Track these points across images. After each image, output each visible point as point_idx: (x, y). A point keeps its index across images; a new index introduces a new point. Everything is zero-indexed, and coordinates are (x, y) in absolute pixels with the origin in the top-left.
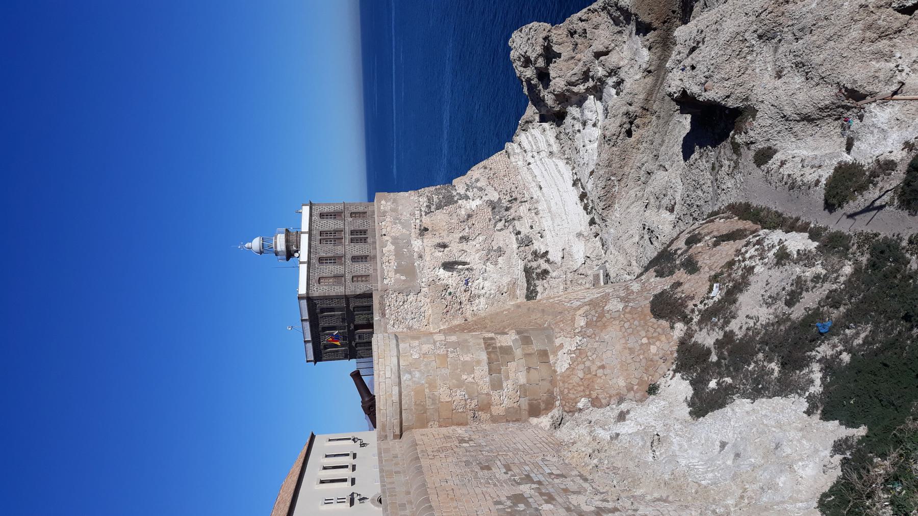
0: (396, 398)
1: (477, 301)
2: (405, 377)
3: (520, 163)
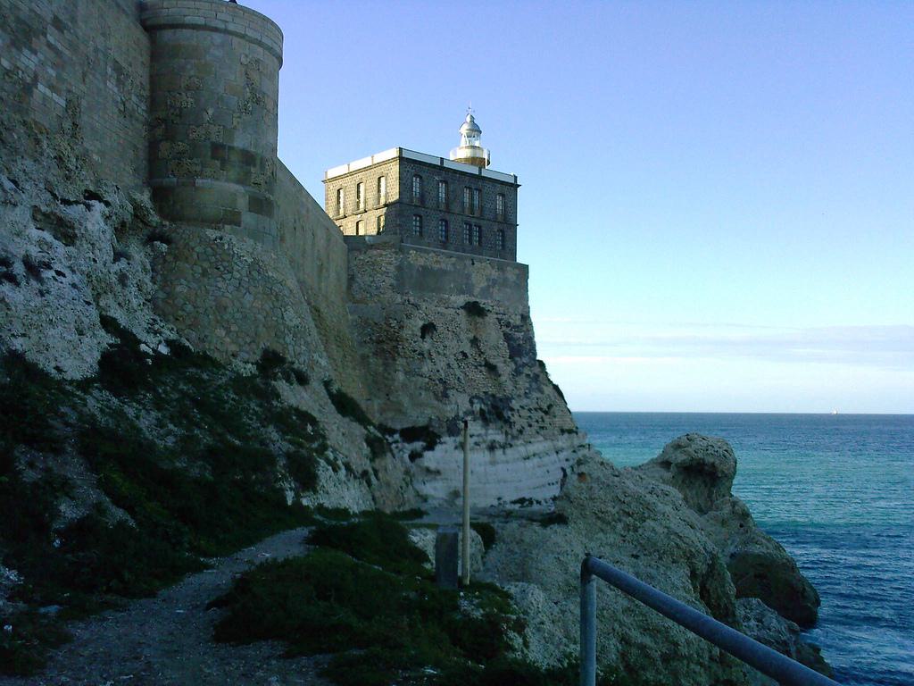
0: (188, 20)
2: (218, 38)
3: (560, 444)
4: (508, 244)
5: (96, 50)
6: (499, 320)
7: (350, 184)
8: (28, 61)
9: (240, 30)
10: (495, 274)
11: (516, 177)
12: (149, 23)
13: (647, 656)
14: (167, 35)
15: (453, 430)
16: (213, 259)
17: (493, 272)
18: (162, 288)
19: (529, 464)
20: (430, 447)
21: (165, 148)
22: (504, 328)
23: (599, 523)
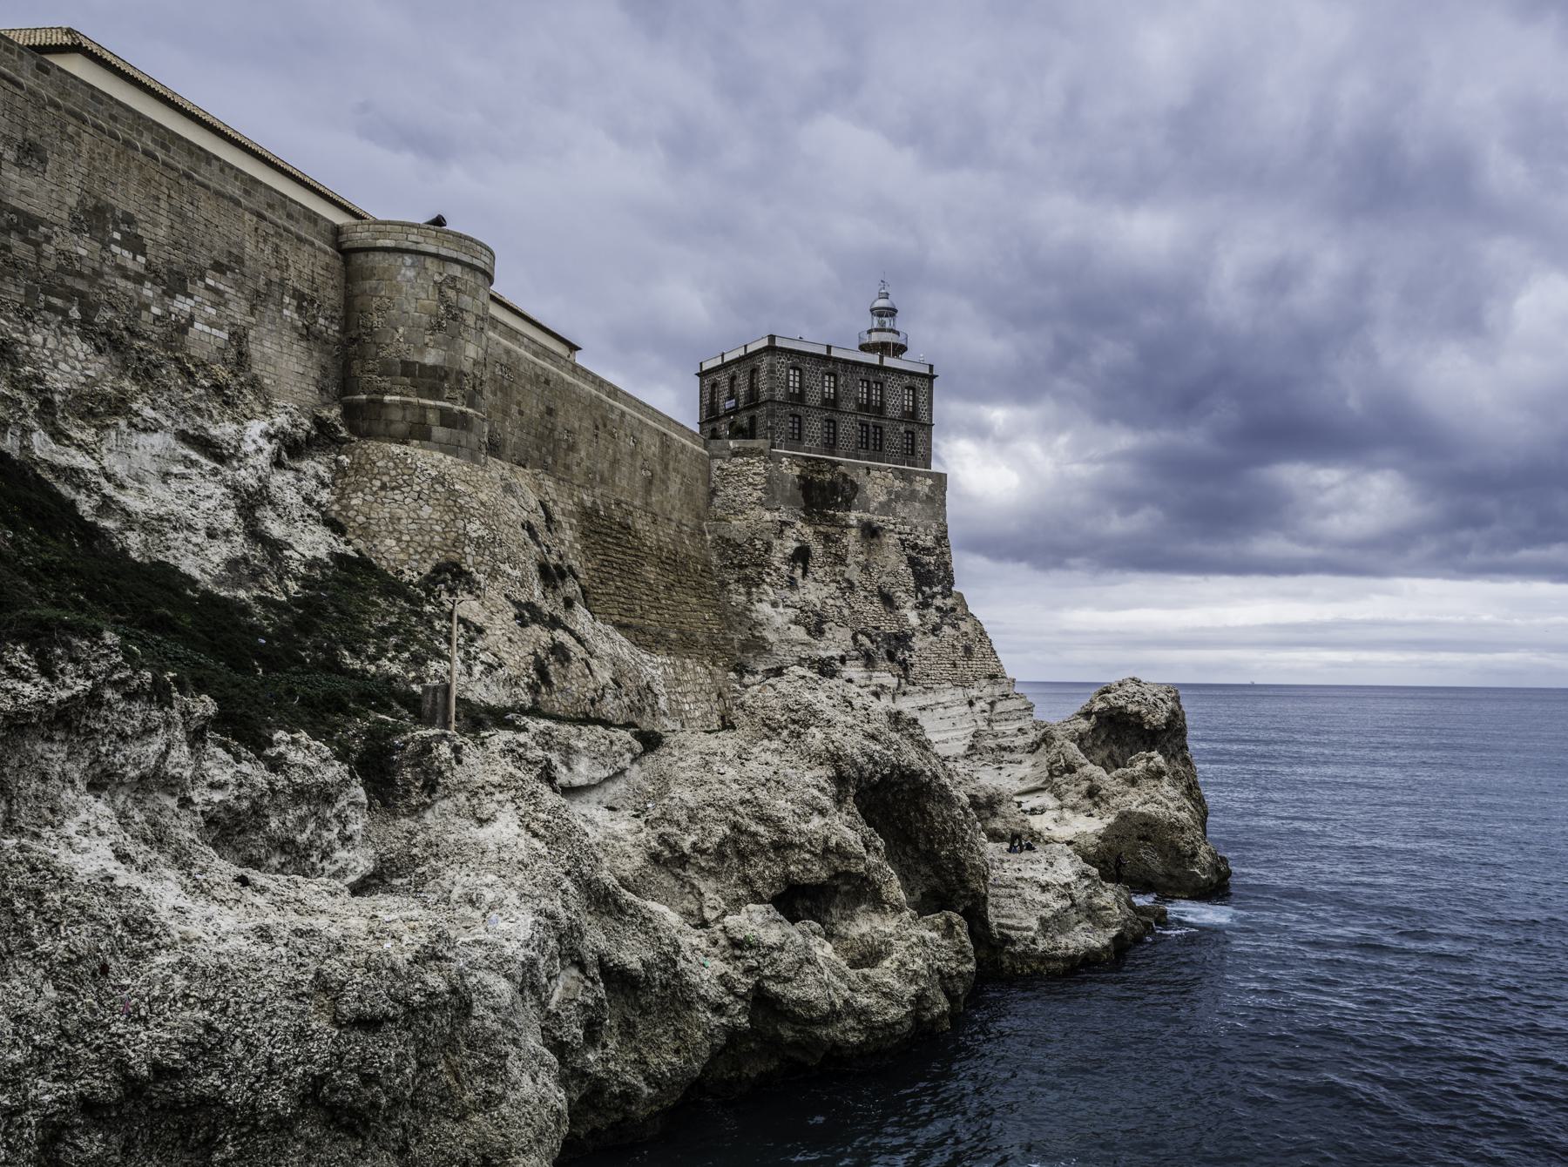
1: (742, 590)
2: (408, 260)
3: (974, 693)
4: (920, 449)
5: (269, 283)
6: (903, 542)
7: (723, 379)
8: (182, 305)
9: (432, 249)
10: (898, 485)
11: (931, 367)
12: (346, 246)
13: (757, 843)
14: (361, 258)
16: (393, 473)
17: (897, 483)
18: (338, 501)
21: (356, 364)
22: (909, 551)
23: (765, 730)
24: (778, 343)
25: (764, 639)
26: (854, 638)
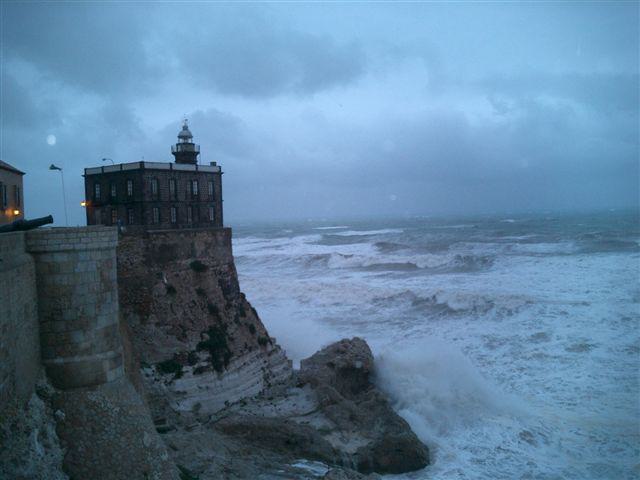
15: (192, 360)
19: (242, 372)
20: (179, 375)
24: (146, 166)
25: (152, 344)
26: (202, 337)
